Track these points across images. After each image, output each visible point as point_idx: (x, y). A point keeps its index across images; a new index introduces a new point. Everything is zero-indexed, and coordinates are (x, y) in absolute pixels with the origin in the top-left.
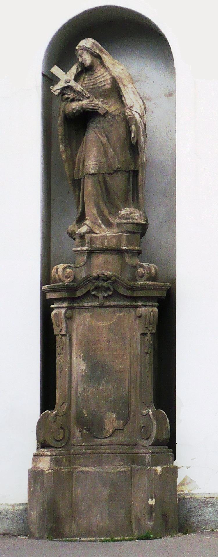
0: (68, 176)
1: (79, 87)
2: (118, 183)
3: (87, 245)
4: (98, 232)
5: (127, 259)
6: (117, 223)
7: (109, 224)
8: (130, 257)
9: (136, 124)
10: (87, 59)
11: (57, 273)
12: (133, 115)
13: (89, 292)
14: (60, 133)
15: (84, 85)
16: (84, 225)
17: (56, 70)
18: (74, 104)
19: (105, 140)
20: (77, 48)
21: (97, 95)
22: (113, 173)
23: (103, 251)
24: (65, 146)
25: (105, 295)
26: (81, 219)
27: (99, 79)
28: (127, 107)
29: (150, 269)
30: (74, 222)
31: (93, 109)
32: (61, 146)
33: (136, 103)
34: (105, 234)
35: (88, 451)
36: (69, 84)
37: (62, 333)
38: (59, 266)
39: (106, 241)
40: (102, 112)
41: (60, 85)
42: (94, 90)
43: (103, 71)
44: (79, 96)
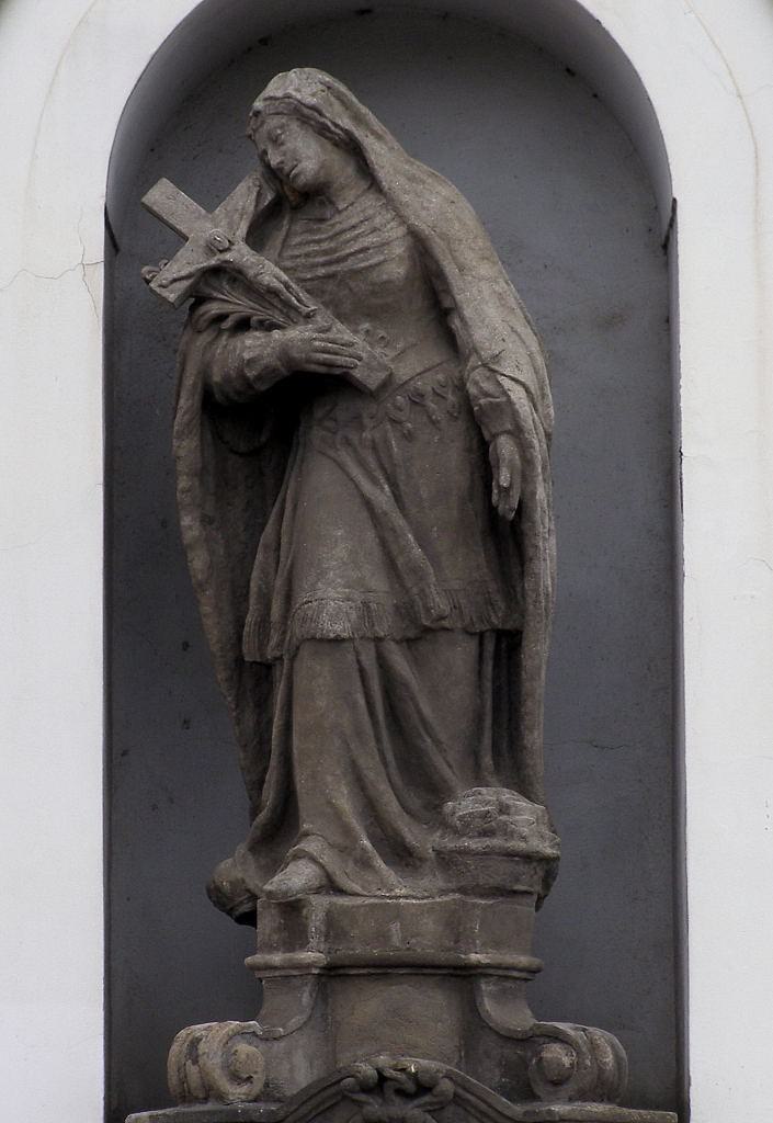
0: (215, 648)
1: (268, 271)
2: (446, 690)
3: (313, 942)
4: (357, 888)
5: (488, 1006)
6: (438, 853)
7: (402, 855)
8: (501, 997)
9: (517, 432)
10: (308, 157)
11: (195, 1062)
12: (505, 393)
14: (181, 467)
15: (288, 264)
16: (296, 857)
17: (164, 196)
18: (248, 342)
19: (382, 497)
20: (258, 104)
21: (347, 307)
22: (417, 639)
23: (385, 969)
24: (206, 521)
26: (278, 831)
27: (356, 238)
28: (473, 361)
29: (594, 1046)
30: (242, 849)
31: (330, 365)
32: (186, 521)
33: (511, 345)
34: (406, 904)
36: (228, 256)
38: (198, 1029)
39: (395, 928)
40: (372, 380)
41: (187, 262)
42: (330, 286)
43: (370, 203)
44: (273, 307)
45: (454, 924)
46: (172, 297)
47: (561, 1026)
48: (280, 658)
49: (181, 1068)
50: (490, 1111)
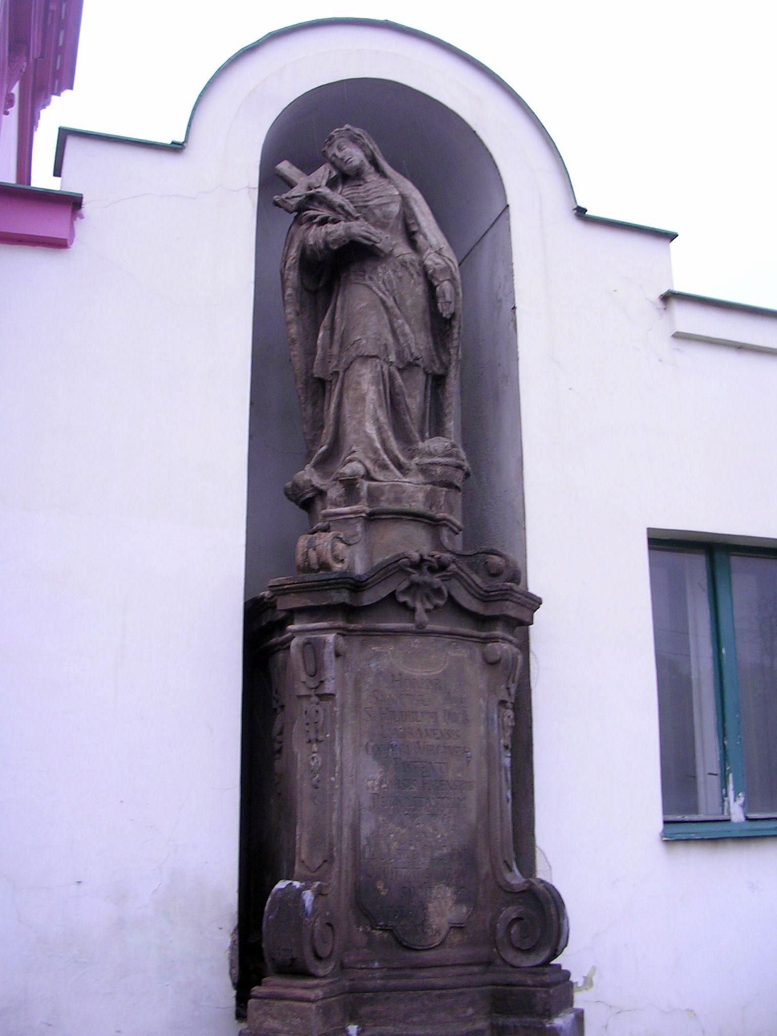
1: (337, 197)
4: (381, 478)
13: (393, 595)
17: (285, 167)
25: (429, 606)
35: (393, 983)
37: (320, 692)
41: (299, 191)
44: (340, 213)
45: (431, 499)
48: (337, 373)
50: (473, 584)
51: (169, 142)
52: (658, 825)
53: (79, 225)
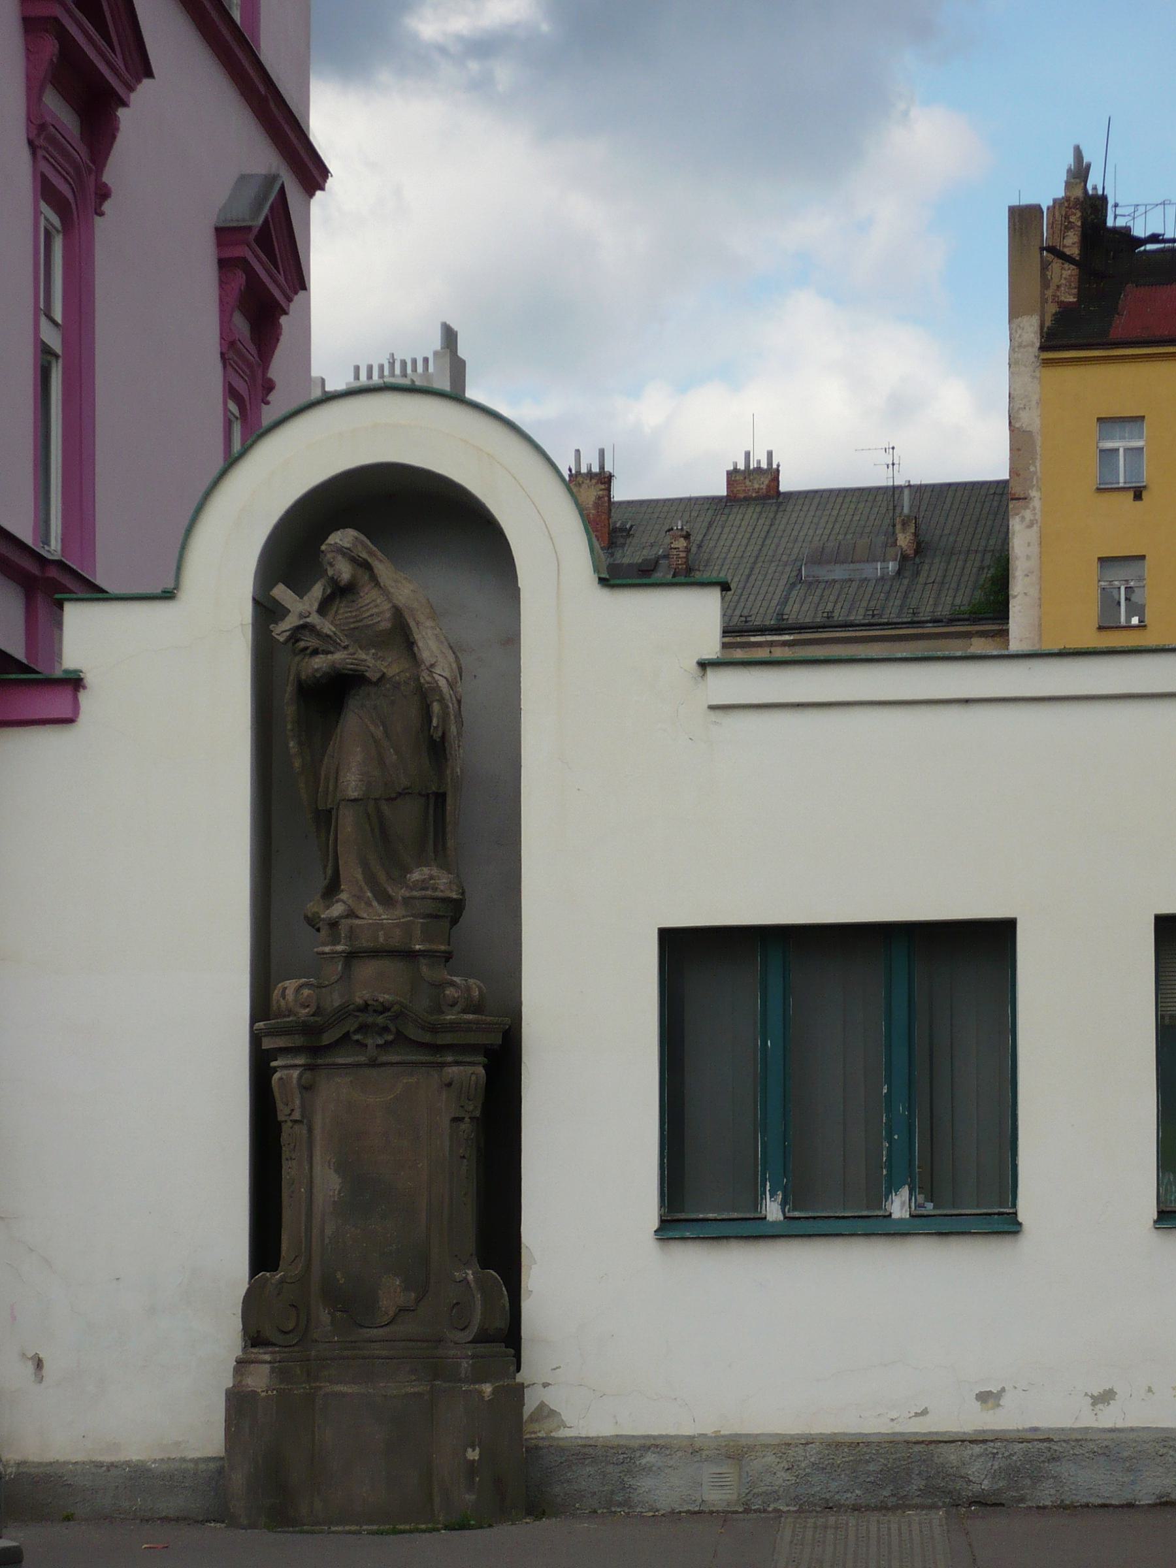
1: (327, 627)
2: (406, 817)
4: (365, 915)
6: (404, 898)
7: (387, 900)
9: (441, 700)
10: (344, 571)
12: (436, 682)
13: (347, 1035)
17: (281, 592)
19: (379, 732)
20: (323, 547)
22: (395, 799)
23: (376, 953)
26: (332, 890)
28: (423, 667)
32: (292, 744)
35: (345, 1353)
36: (308, 620)
44: (328, 643)
46: (282, 639)
47: (455, 979)
49: (278, 1001)
51: (159, 591)
52: (655, 1224)
53: (83, 697)
